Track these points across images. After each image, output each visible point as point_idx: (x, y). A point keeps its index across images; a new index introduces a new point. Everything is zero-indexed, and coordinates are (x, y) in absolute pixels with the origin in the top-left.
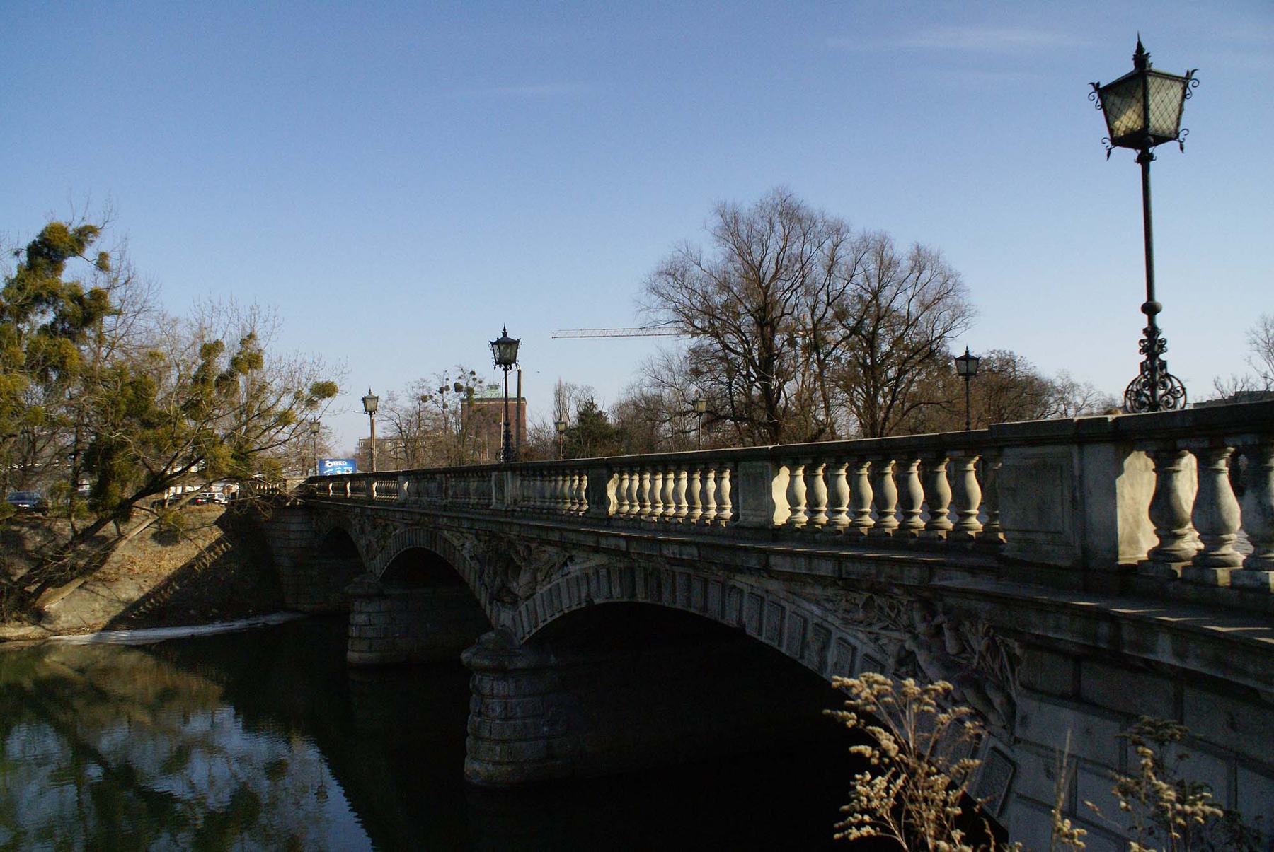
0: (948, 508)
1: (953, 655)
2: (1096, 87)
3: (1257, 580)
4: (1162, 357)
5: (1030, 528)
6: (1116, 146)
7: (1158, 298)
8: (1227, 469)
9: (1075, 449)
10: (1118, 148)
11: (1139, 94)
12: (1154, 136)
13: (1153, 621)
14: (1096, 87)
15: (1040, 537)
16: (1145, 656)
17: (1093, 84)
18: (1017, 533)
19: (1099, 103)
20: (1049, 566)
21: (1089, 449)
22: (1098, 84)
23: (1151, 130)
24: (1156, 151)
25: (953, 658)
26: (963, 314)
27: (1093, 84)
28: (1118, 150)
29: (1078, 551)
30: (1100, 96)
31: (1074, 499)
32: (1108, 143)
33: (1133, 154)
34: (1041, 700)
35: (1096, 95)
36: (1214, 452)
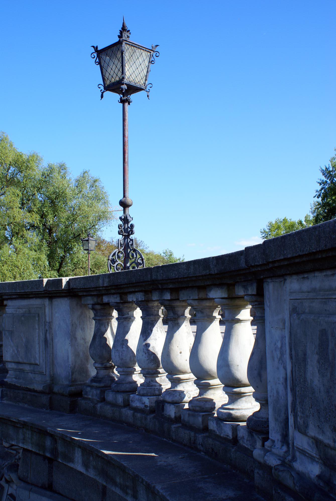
0: (215, 317)
1: (8, 448)
2: (96, 48)
3: (143, 404)
4: (132, 237)
5: (21, 360)
6: (107, 90)
7: (130, 198)
8: (162, 316)
9: (47, 301)
10: (108, 92)
11: (119, 55)
12: (128, 85)
13: (68, 439)
14: (96, 48)
15: (27, 368)
16: (66, 464)
17: (93, 47)
18: (13, 364)
19: (97, 60)
20: (30, 390)
21: (54, 300)
22: (97, 47)
23: (126, 81)
24: (133, 97)
25: (6, 450)
26: (106, 218)
27: (93, 47)
28: (108, 94)
29: (48, 379)
30: (98, 56)
31: (46, 341)
32: (102, 88)
33: (117, 97)
34: (30, 490)
35: (95, 55)
36: (126, 305)
